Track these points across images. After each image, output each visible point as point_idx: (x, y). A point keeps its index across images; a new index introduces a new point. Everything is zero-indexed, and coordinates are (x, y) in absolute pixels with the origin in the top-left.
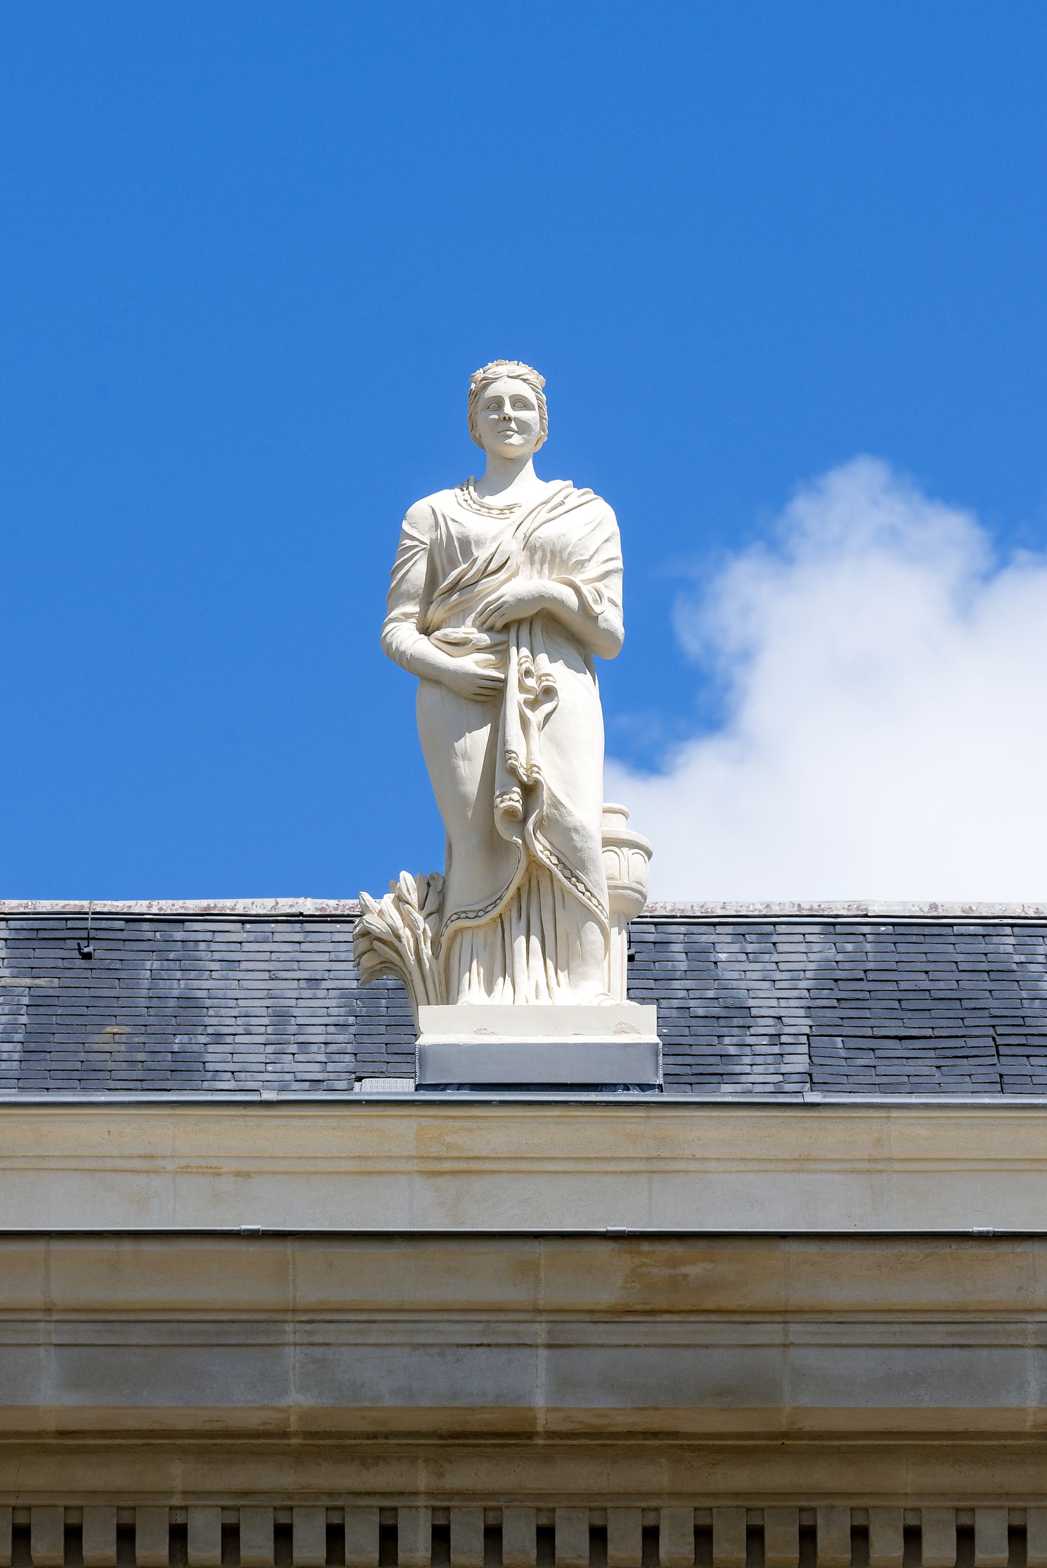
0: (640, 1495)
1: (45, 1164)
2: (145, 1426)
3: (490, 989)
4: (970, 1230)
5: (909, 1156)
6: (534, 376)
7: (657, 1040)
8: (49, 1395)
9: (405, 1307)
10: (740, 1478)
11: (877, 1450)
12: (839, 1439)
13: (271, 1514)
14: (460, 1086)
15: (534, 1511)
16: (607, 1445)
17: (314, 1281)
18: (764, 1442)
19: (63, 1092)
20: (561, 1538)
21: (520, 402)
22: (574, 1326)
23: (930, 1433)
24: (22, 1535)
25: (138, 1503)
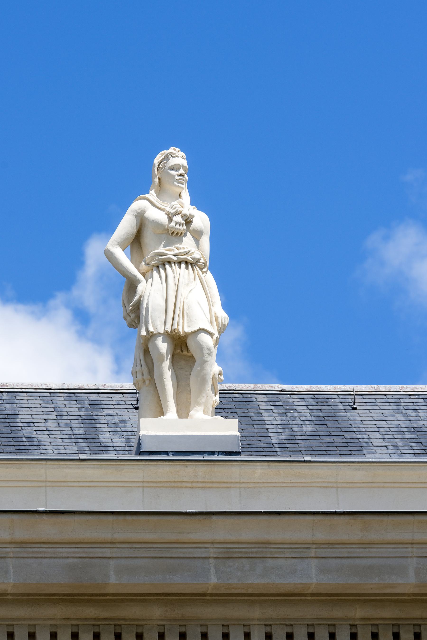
0: (244, 620)
3: (183, 412)
5: (92, 480)
7: (238, 433)
8: (8, 580)
9: (375, 542)
11: (123, 601)
12: (103, 596)
14: (219, 453)
15: (412, 626)
16: (158, 599)
17: (278, 532)
23: (402, 594)
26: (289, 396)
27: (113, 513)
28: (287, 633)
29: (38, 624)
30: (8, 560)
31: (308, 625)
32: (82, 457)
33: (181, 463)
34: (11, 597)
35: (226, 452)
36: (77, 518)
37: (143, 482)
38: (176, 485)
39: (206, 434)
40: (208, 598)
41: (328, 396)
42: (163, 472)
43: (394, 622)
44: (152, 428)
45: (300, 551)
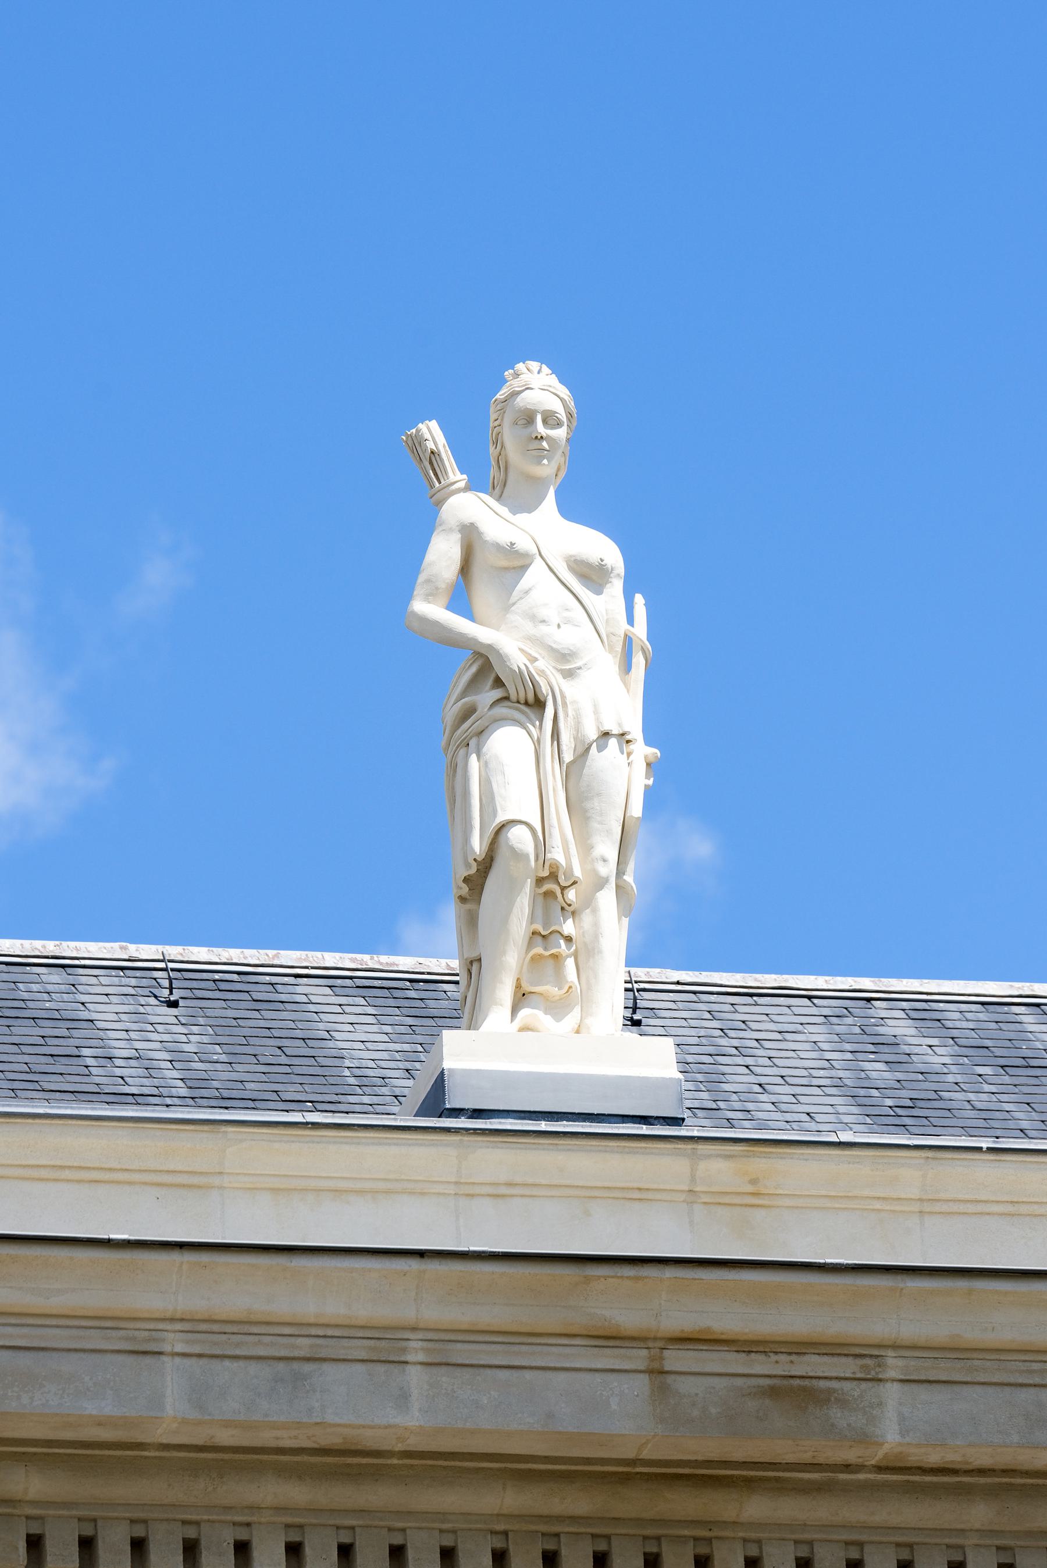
1: (1010, 1208)
2: (200, 1442)
4: (822, 1261)
6: (564, 392)
10: (634, 1504)
13: (791, 1547)
15: (437, 1533)
18: (157, 1454)
19: (117, 1107)
20: (50, 1547)
21: (550, 419)
22: (459, 1346)
24: (35, 1543)
25: (255, 1519)
26: (408, 983)
27: (181, 1246)
28: (186, 1541)
29: (666, 1536)
30: (164, 1358)
31: (79, 1519)
32: (846, 1137)
33: (594, 1142)
34: (157, 1454)
35: (664, 1118)
36: (669, 1273)
37: (920, 1200)
38: (927, 1206)
39: (562, 1071)
40: (395, 1461)
41: (275, 979)
42: (493, 1161)
43: (290, 1520)
44: (481, 1053)
45: (382, 1347)
